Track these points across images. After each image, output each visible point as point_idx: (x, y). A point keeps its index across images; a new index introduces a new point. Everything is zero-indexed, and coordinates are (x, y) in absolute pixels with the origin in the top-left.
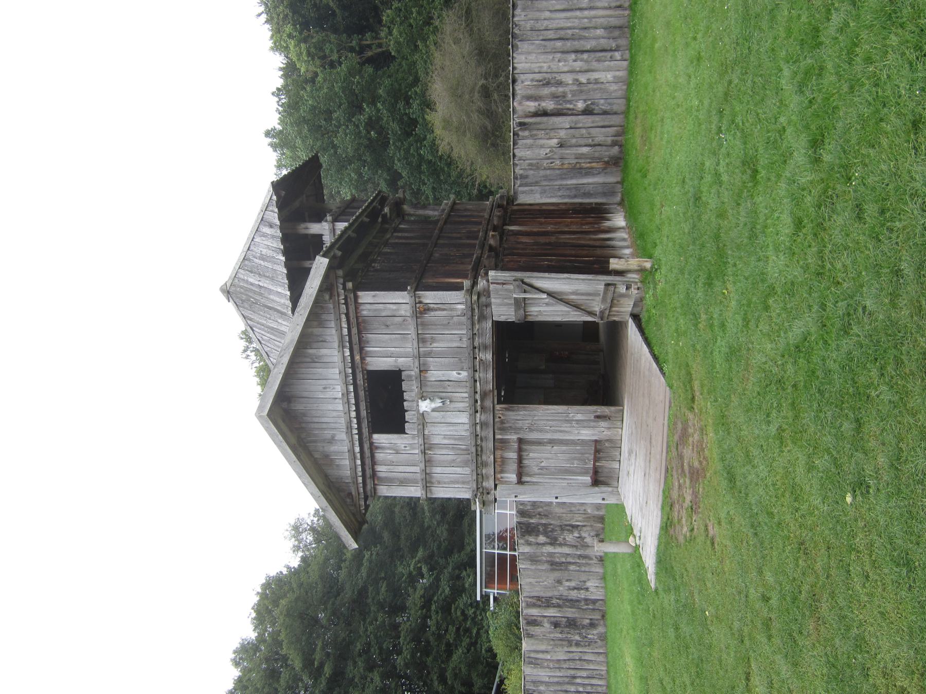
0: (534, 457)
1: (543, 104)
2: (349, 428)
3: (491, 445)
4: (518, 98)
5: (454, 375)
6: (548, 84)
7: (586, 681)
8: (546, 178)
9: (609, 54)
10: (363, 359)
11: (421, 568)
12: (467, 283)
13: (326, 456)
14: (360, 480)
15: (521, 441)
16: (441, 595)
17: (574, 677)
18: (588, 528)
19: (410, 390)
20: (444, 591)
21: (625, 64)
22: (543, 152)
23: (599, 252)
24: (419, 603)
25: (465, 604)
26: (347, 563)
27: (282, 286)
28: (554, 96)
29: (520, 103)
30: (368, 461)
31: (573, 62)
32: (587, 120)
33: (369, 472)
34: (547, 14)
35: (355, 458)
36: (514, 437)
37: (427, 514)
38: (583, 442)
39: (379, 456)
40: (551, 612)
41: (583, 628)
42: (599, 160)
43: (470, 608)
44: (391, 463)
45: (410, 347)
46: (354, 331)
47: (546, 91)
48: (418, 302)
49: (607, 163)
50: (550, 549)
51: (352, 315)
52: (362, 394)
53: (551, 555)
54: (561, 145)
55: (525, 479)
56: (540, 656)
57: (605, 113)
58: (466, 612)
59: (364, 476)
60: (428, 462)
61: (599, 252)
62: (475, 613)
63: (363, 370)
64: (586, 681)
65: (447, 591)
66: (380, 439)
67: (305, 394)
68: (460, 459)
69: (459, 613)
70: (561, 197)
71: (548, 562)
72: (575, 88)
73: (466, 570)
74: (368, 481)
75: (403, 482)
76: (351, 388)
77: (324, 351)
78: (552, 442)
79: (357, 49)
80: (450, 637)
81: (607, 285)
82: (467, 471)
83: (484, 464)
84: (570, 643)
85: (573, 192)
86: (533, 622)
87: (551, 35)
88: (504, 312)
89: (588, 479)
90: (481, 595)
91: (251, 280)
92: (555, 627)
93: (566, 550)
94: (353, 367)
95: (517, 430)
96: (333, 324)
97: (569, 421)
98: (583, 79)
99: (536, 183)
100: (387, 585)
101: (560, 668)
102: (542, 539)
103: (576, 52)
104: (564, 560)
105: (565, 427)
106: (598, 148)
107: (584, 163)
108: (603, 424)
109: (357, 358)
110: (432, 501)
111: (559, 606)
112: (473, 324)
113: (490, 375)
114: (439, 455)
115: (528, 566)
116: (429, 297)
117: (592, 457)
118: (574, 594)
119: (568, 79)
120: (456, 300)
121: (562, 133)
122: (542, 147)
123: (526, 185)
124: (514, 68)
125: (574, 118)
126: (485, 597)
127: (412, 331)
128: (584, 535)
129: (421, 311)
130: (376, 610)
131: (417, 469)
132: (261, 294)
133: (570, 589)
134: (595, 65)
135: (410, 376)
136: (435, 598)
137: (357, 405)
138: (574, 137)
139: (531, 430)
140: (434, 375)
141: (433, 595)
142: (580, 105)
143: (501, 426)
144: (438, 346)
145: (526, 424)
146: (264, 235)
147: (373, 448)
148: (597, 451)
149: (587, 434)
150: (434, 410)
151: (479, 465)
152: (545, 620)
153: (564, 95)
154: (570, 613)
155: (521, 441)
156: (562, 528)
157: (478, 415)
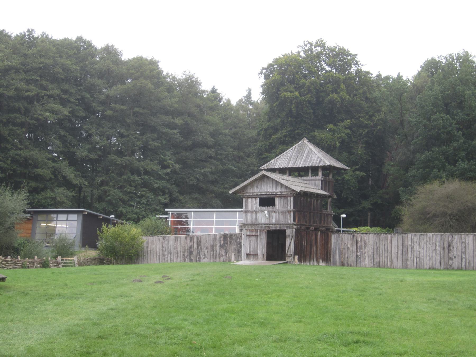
0: (254, 239)
1: (359, 243)
2: (260, 192)
3: (257, 228)
4: (361, 235)
5: (274, 219)
6: (365, 244)
7: (169, 258)
8: (339, 244)
9: (372, 262)
10: (278, 197)
11: (169, 168)
12: (295, 223)
13: (253, 186)
14: (247, 194)
15: (258, 236)
16: (154, 181)
17: (171, 254)
18: (226, 258)
19: (270, 208)
20: (156, 183)
22: (346, 243)
23: (308, 257)
24: (148, 168)
25: (148, 197)
26: (172, 120)
27: (303, 165)
29: (360, 236)
30: (252, 196)
32: (355, 256)
33: (249, 196)
34: (383, 244)
35: (253, 193)
36: (259, 234)
37: (203, 170)
38: (257, 251)
39: (253, 199)
40: (195, 246)
41: (189, 257)
42: (344, 260)
43: (146, 200)
44: (251, 202)
45: (280, 209)
46: (284, 195)
47: (363, 243)
49: (343, 262)
50: (218, 245)
51: (288, 195)
52: (269, 196)
53: (216, 245)
54: (348, 248)
55: (248, 237)
56: (179, 242)
57: (357, 261)
58: (144, 198)
59: (248, 195)
60: (252, 212)
61: (308, 257)
62: (143, 203)
63: (275, 197)
64: (169, 258)
65: (156, 186)
66: (258, 200)
67: (269, 182)
68: (253, 220)
69: (143, 193)
70: (333, 248)
71: (214, 244)
72: (364, 252)
73: (168, 197)
74: (247, 196)
75: (247, 205)
76: (270, 194)
77: (279, 188)
78: (257, 244)
80: (127, 189)
81: (292, 255)
82: (250, 222)
83: (252, 227)
84: (184, 252)
85: (334, 252)
87: (378, 245)
88: (289, 232)
89: (248, 253)
90: (167, 211)
91: (306, 151)
92: (190, 247)
93: (218, 251)
94: (275, 194)
95: (260, 235)
96: (286, 190)
97: (263, 248)
98: (366, 255)
99: (337, 240)
100: (158, 146)
101: (174, 249)
102: (222, 242)
103: (373, 252)
104: (215, 250)
105: (261, 247)
106: (347, 260)
108: (262, 256)
109: (278, 196)
111: (198, 248)
112: (286, 224)
113: (274, 228)
114: (254, 215)
115: (212, 238)
116: (292, 214)
117: (254, 253)
118: (202, 254)
119: (366, 250)
120: (291, 221)
121: (351, 249)
122: (348, 242)
123: (337, 237)
124: (370, 234)
125: (356, 252)
126: (166, 213)
127: (284, 209)
128: (224, 257)
129: (289, 212)
130: (143, 140)
131: (250, 209)
132: (301, 155)
133: (204, 252)
134: (370, 258)
135: (273, 208)
136: (152, 178)
137: (266, 195)
138: (350, 252)
139: (260, 238)
140: (274, 214)
141: (153, 176)
142: (359, 254)
144: (281, 216)
145: (262, 237)
146: (317, 159)
147: (255, 198)
148: (255, 255)
149: (259, 252)
150: (265, 214)
152: (192, 244)
153: (362, 249)
154: (195, 253)
155: (258, 236)
156: (226, 249)
157: (264, 225)
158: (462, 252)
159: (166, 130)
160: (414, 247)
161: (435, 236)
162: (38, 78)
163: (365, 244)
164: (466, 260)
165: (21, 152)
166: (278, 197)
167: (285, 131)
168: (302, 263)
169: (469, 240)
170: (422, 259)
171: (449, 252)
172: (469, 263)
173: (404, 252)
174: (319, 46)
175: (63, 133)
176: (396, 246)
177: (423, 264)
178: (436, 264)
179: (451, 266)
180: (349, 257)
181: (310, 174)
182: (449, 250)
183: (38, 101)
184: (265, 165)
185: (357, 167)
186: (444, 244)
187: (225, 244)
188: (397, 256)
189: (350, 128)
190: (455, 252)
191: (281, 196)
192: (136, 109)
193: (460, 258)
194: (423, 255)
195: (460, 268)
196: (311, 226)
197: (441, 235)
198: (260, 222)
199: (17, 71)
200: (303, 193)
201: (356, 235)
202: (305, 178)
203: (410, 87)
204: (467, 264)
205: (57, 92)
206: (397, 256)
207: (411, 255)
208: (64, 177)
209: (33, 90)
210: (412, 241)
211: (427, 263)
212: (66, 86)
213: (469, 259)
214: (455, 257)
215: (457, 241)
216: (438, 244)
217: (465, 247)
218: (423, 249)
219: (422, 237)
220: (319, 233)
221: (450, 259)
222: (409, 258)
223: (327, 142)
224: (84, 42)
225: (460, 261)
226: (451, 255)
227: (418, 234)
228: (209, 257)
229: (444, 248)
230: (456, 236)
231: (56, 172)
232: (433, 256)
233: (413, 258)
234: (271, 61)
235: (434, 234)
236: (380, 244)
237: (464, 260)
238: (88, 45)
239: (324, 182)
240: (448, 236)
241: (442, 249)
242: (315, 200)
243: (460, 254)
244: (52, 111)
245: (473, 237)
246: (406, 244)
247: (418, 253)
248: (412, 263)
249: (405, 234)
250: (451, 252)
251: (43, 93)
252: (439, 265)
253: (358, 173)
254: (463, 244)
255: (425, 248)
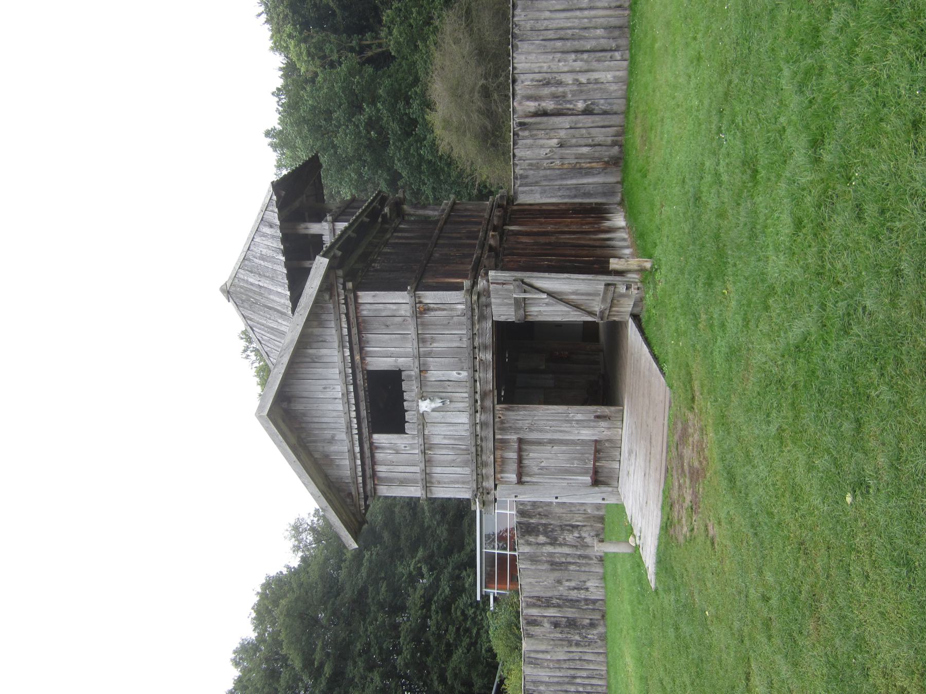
0: (534, 457)
1: (543, 104)
2: (349, 428)
3: (491, 445)
4: (518, 98)
5: (454, 375)
6: (548, 84)
7: (586, 681)
8: (546, 178)
9: (609, 54)
10: (363, 359)
11: (421, 568)
12: (467, 283)
13: (326, 456)
14: (360, 480)
15: (521, 441)
16: (441, 595)
17: (574, 677)
18: (588, 528)
19: (410, 390)
20: (444, 591)
21: (625, 64)
22: (543, 152)
23: (599, 252)
24: (419, 603)
25: (465, 604)
26: (347, 563)
27: (282, 286)
28: (554, 96)
29: (520, 103)
30: (368, 461)
31: (573, 62)
32: (587, 120)
33: (369, 472)
34: (547, 14)
35: (355, 458)
36: (514, 437)
37: (427, 514)
38: (583, 442)
39: (379, 456)
40: (551, 612)
41: (583, 628)
42: (599, 160)
43: (470, 608)
44: (391, 463)
45: (410, 347)
46: (354, 331)
47: (546, 91)
48: (418, 302)
49: (607, 163)
50: (550, 549)
51: (352, 315)
52: (362, 394)
53: (551, 555)
54: (561, 145)
55: (525, 479)
56: (540, 656)
57: (605, 113)
58: (466, 612)
59: (364, 476)
60: (428, 462)
61: (599, 252)
62: (475, 613)
63: (363, 370)
64: (586, 681)
65: (447, 591)
66: (380, 439)
67: (305, 394)
68: (460, 459)
69: (459, 613)
70: (561, 197)
71: (548, 562)
72: (575, 88)
73: (466, 570)
74: (368, 481)
75: (403, 482)
76: (351, 388)
77: (324, 351)
78: (552, 442)
79: (357, 49)
80: (450, 637)
81: (607, 285)
82: (467, 471)
83: (484, 464)
84: (570, 643)
85: (573, 192)
86: (533, 622)
87: (551, 35)
88: (504, 312)
89: (588, 479)
90: (481, 595)
91: (251, 280)
92: (555, 627)
93: (566, 550)
94: (353, 367)
95: (517, 430)
96: (333, 324)
97: (569, 421)
98: (583, 79)
99: (536, 183)
100: (387, 585)
101: (560, 668)
102: (542, 539)
103: (576, 52)
104: (564, 560)
105: (565, 427)
106: (598, 148)
107: (584, 163)
108: (603, 424)
109: (357, 358)
110: (432, 501)
111: (559, 606)
112: (473, 324)
113: (490, 375)
114: (439, 455)
115: (528, 566)
116: (429, 297)
117: (592, 457)
118: (574, 594)
119: (568, 79)
120: (456, 300)
121: (562, 133)
122: (542, 147)
123: (526, 185)
124: (514, 68)
125: (574, 118)
126: (485, 597)
127: (412, 331)
128: (584, 535)
129: (421, 311)
130: (376, 610)
131: (417, 469)
132: (261, 294)
133: (570, 589)
134: (595, 65)
135: (410, 376)
136: (435, 598)
137: (357, 405)
138: (574, 137)
139: (531, 430)
140: (434, 375)
141: (433, 595)
142: (580, 105)
143: (501, 426)
144: (438, 346)
145: (526, 424)
146: (264, 235)
147: (373, 448)
148: (597, 451)
149: (587, 434)
150: (434, 410)
151: (479, 465)
152: (545, 620)
153: (564, 95)
154: (570, 613)
155: (521, 441)
156: (562, 528)
157: (478, 415)
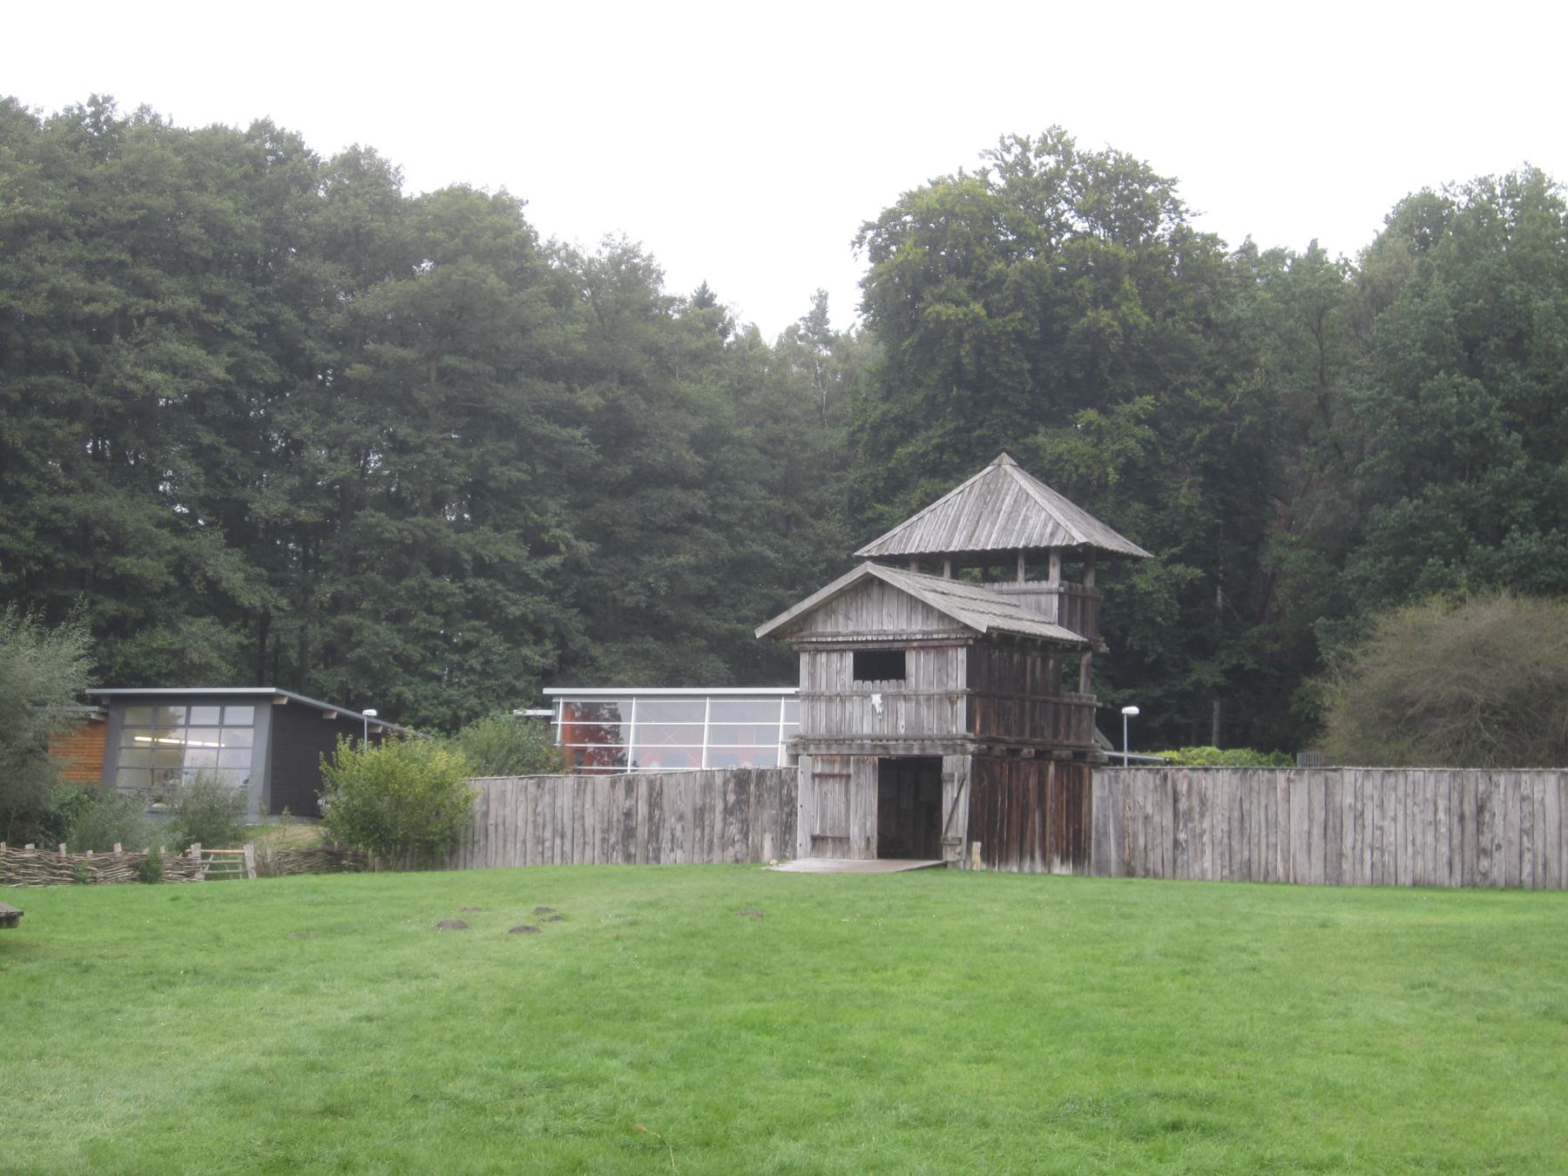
0: (835, 787)
1: (1184, 799)
2: (858, 634)
3: (845, 752)
4: (1190, 774)
5: (902, 723)
6: (1203, 802)
7: (557, 851)
8: (1115, 803)
9: (1227, 864)
10: (914, 648)
11: (558, 552)
12: (971, 735)
13: (834, 612)
14: (814, 639)
15: (848, 777)
16: (506, 597)
17: (563, 837)
18: (745, 851)
19: (890, 686)
20: (515, 603)
22: (1140, 799)
23: (1015, 846)
24: (489, 554)
25: (488, 649)
26: (566, 396)
27: (997, 542)
29: (1185, 776)
30: (830, 647)
32: (1169, 843)
33: (820, 647)
34: (1263, 804)
35: (833, 636)
36: (852, 771)
37: (669, 561)
38: (848, 828)
39: (835, 657)
40: (642, 810)
41: (624, 846)
42: (1132, 856)
43: (482, 660)
44: (828, 666)
45: (924, 688)
46: (936, 643)
47: (1195, 802)
49: (1129, 864)
50: (720, 806)
51: (948, 642)
52: (886, 646)
53: (713, 809)
54: (1147, 818)
55: (817, 780)
56: (589, 796)
57: (1175, 861)
58: (474, 652)
59: (817, 642)
60: (830, 699)
61: (1015, 846)
62: (472, 669)
63: (906, 648)
64: (557, 851)
65: (514, 611)
66: (849, 659)
67: (886, 599)
68: (833, 725)
69: (470, 636)
70: (1098, 818)
71: (704, 804)
72: (1198, 831)
73: (554, 649)
74: (812, 646)
75: (812, 676)
76: (891, 638)
77: (920, 618)
78: (848, 802)
80: (419, 622)
81: (960, 839)
82: (823, 731)
83: (829, 747)
84: (606, 831)
85: (1102, 831)
87: (1246, 806)
88: (950, 764)
89: (817, 832)
90: (551, 696)
91: (1008, 498)
92: (625, 814)
93: (718, 826)
94: (907, 640)
95: (858, 774)
96: (941, 627)
97: (865, 817)
98: (1206, 838)
99: (1111, 792)
100: (520, 482)
101: (574, 820)
102: (732, 798)
103: (1230, 832)
104: (707, 823)
105: (860, 813)
106: (1143, 855)
108: (863, 844)
109: (915, 644)
111: (651, 818)
112: (941, 739)
113: (901, 752)
114: (836, 708)
115: (698, 783)
116: (961, 706)
117: (836, 835)
118: (666, 835)
119: (1206, 825)
120: (960, 727)
121: (1157, 819)
122: (1145, 798)
123: (1110, 782)
124: (1218, 770)
125: (1171, 830)
126: (547, 702)
127: (935, 689)
128: (737, 846)
129: (951, 698)
130: (472, 460)
131: (823, 688)
132: (992, 511)
133: (673, 831)
134: (1218, 850)
135: (900, 686)
136: (499, 587)
137: (877, 641)
138: (1154, 830)
139: (857, 785)
140: (902, 706)
141: (503, 580)
142: (1182, 836)
144: (924, 710)
145: (862, 780)
146: (1045, 524)
147: (841, 651)
148: (840, 839)
149: (854, 831)
150: (873, 707)
152: (633, 802)
153: (1191, 820)
154: (642, 832)
155: (848, 777)
156: (745, 821)
157: (869, 742)
158: (1521, 830)
159: (548, 429)
160: (1362, 813)
161: (1432, 779)
162: (125, 257)
163: (1203, 802)
164: (1535, 856)
165: (68, 501)
166: (914, 648)
167: (940, 432)
168: (994, 865)
169: (1544, 791)
170: (1390, 852)
171: (1479, 831)
172: (1545, 866)
173: (1330, 831)
174: (1052, 151)
175: (207, 439)
176: (1306, 812)
177: (1392, 870)
178: (1435, 869)
179: (1485, 875)
180: (1149, 847)
181: (1021, 575)
182: (1478, 823)
183: (126, 333)
184: (874, 543)
185: (1175, 550)
186: (1461, 803)
187: (742, 803)
188: (1309, 845)
189: (1152, 421)
190: (1499, 831)
191: (927, 645)
192: (450, 360)
193: (1515, 850)
194: (1392, 839)
195: (1516, 883)
196: (1024, 743)
197: (1454, 775)
198: (856, 730)
199: (56, 233)
200: (999, 635)
201: (1172, 775)
202: (1005, 586)
203: (1349, 285)
204: (1540, 869)
205: (187, 303)
206: (1309, 845)
207: (1355, 840)
208: (212, 584)
209: (109, 298)
210: (1358, 795)
211: (1407, 865)
212: (218, 285)
213: (1545, 854)
214: (1499, 847)
215: (1505, 794)
216: (1442, 804)
217: (1532, 814)
218: (1395, 819)
219: (1391, 780)
220: (1052, 769)
221: (1484, 852)
222: (1347, 850)
223: (1077, 467)
224: (278, 138)
225: (1515, 860)
226: (1485, 841)
227: (1377, 772)
228: (687, 846)
229: (1462, 818)
230: (1503, 779)
231: (183, 567)
232: (1425, 844)
233: (1362, 849)
234: (892, 202)
235: (1430, 772)
236: (1251, 802)
237: (1528, 856)
238: (292, 147)
239: (1066, 599)
240: (1474, 779)
241: (1456, 819)
242: (1039, 660)
243: (1514, 835)
244: (172, 367)
245: (1559, 781)
246: (1338, 805)
247: (1378, 833)
248: (1358, 867)
249: (1334, 770)
250: (1486, 830)
251: (142, 305)
252: (1446, 872)
253: (1178, 569)
254: (1525, 805)
255: (1400, 817)
